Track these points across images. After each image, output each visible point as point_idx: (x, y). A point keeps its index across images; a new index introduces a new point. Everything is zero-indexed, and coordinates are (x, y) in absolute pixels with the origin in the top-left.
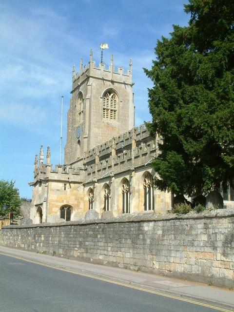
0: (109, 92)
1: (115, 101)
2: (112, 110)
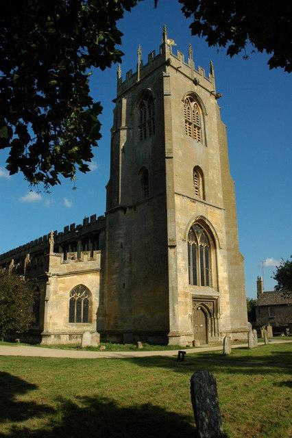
2: (195, 126)
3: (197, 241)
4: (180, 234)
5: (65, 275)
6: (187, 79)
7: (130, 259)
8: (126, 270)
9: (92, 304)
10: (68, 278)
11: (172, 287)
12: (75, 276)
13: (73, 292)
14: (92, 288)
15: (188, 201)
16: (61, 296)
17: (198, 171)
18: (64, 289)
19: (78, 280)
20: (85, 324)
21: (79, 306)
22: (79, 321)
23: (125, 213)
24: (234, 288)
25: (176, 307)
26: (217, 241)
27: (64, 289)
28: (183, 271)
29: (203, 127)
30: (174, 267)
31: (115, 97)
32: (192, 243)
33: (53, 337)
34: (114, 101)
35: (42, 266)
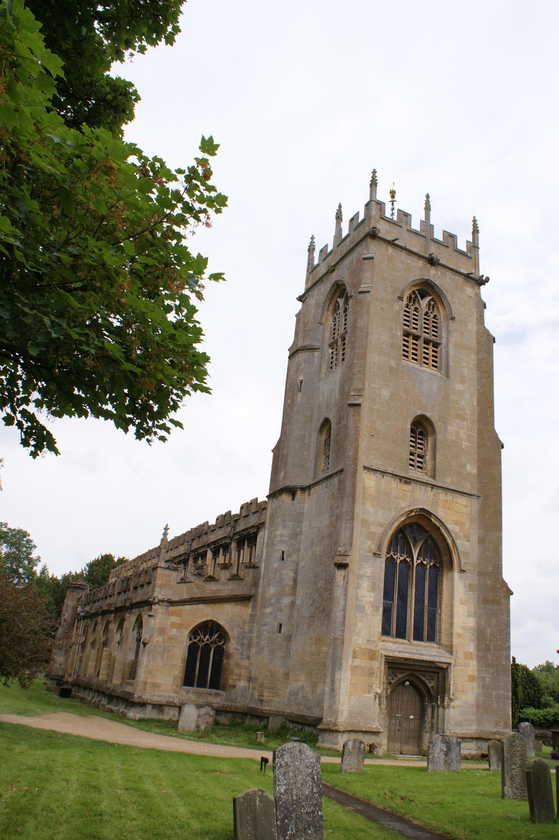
1: (435, 317)
2: (427, 342)
3: (411, 557)
4: (369, 543)
6: (415, 259)
7: (295, 581)
8: (286, 600)
9: (229, 656)
10: (187, 607)
12: (201, 606)
13: (194, 632)
14: (232, 629)
15: (394, 483)
16: (172, 639)
18: (179, 627)
20: (213, 691)
22: (202, 684)
23: (293, 499)
24: (488, 649)
25: (337, 676)
26: (454, 556)
27: (179, 627)
28: (369, 610)
29: (444, 341)
30: (342, 602)
31: (302, 292)
32: (399, 558)
33: (149, 708)
34: (300, 299)
35: (149, 583)
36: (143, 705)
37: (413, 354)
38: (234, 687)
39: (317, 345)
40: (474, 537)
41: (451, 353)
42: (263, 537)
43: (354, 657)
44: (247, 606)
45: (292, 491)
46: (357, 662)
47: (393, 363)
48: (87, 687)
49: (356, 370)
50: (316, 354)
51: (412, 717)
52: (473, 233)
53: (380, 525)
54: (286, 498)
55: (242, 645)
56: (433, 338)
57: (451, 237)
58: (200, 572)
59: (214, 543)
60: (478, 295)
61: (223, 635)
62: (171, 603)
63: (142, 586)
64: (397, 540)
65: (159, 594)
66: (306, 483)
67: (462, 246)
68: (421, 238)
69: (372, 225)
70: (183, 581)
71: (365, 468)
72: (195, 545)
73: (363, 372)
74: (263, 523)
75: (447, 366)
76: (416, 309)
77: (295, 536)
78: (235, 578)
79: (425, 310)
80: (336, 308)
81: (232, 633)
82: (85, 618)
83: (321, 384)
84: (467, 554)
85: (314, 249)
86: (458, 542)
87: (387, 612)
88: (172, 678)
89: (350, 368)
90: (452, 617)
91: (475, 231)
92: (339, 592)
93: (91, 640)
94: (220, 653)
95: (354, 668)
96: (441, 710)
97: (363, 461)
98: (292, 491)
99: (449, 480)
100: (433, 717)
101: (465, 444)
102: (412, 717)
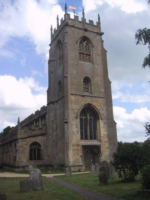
0: (85, 39)
1: (88, 47)
2: (86, 55)
5: (27, 138)
7: (57, 128)
8: (55, 133)
11: (66, 142)
12: (32, 138)
13: (31, 145)
15: (80, 98)
17: (87, 80)
19: (33, 140)
20: (38, 161)
21: (35, 152)
22: (35, 159)
25: (68, 152)
27: (26, 145)
28: (76, 133)
29: (92, 54)
30: (67, 132)
32: (84, 118)
33: (21, 168)
35: (16, 134)
36: (19, 167)
37: (83, 59)
38: (44, 159)
39: (55, 59)
40: (105, 109)
41: (94, 57)
42: (47, 116)
43: (73, 146)
44: (45, 136)
45: (53, 103)
46: (74, 148)
47: (76, 63)
48: (5, 165)
49: (65, 66)
50: (55, 62)
51: (91, 160)
52: (98, 19)
53: (77, 109)
54: (51, 105)
55: (45, 147)
56: (88, 53)
57: (91, 22)
58: (30, 129)
59: (35, 119)
60: (101, 38)
61: (39, 145)
62: (23, 138)
63: (15, 135)
64: (83, 113)
65: (19, 136)
66: (57, 100)
67: (95, 24)
68: (82, 23)
69: (66, 22)
70: (25, 132)
71: (71, 94)
72: (30, 121)
73: (67, 67)
74: (47, 113)
75: (93, 61)
76: (82, 45)
77: (55, 115)
78: (40, 129)
79: (85, 45)
80: (60, 48)
81: (42, 144)
82: (2, 146)
83: (58, 71)
84: (103, 114)
85: (52, 29)
86: (100, 111)
87: (81, 133)
88: (26, 159)
89: (64, 66)
90: (100, 132)
91: (99, 18)
92: (66, 130)
93: (4, 152)
94: (39, 150)
95: (73, 150)
96: (99, 157)
97: (69, 92)
98: (53, 103)
99: (96, 94)
100: (97, 160)
101: (100, 83)
102: (91, 160)
